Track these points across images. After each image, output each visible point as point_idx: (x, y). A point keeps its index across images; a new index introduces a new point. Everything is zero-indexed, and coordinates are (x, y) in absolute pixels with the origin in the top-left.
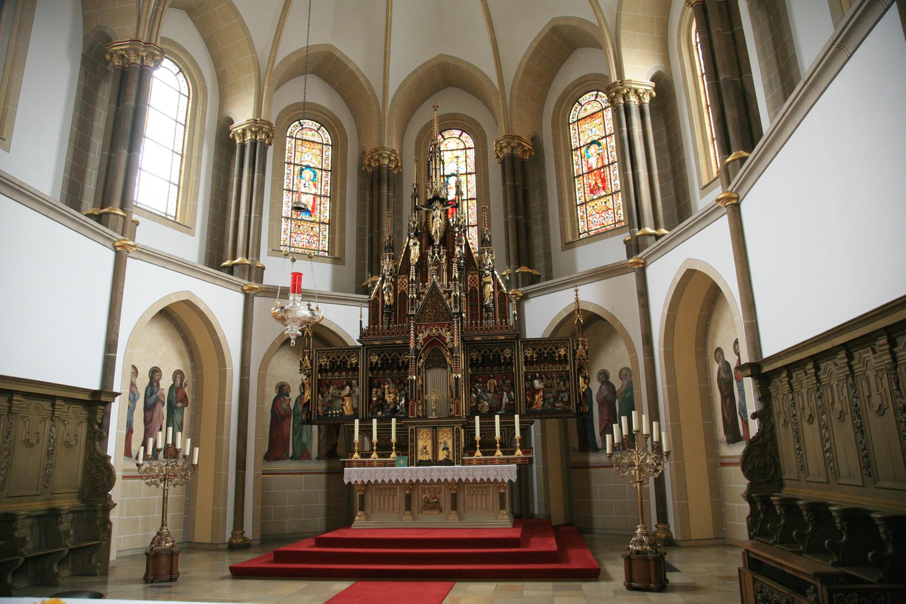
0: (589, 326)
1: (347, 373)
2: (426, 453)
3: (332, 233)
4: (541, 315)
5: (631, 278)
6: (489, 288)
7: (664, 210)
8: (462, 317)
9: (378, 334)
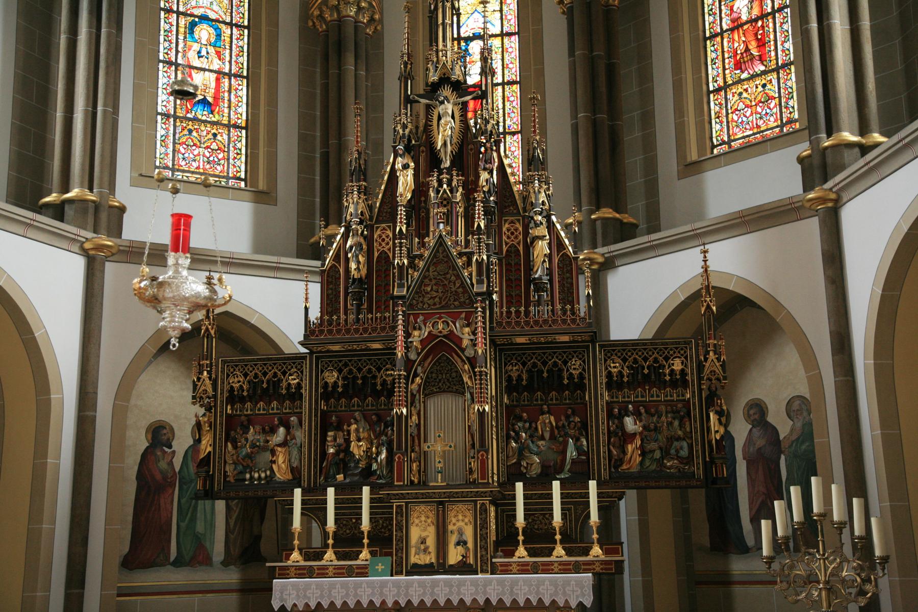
0: (726, 319)
1: (281, 403)
2: (426, 550)
3: (252, 144)
4: (639, 296)
5: (812, 227)
6: (542, 248)
7: (879, 97)
8: (491, 301)
9: (339, 331)
